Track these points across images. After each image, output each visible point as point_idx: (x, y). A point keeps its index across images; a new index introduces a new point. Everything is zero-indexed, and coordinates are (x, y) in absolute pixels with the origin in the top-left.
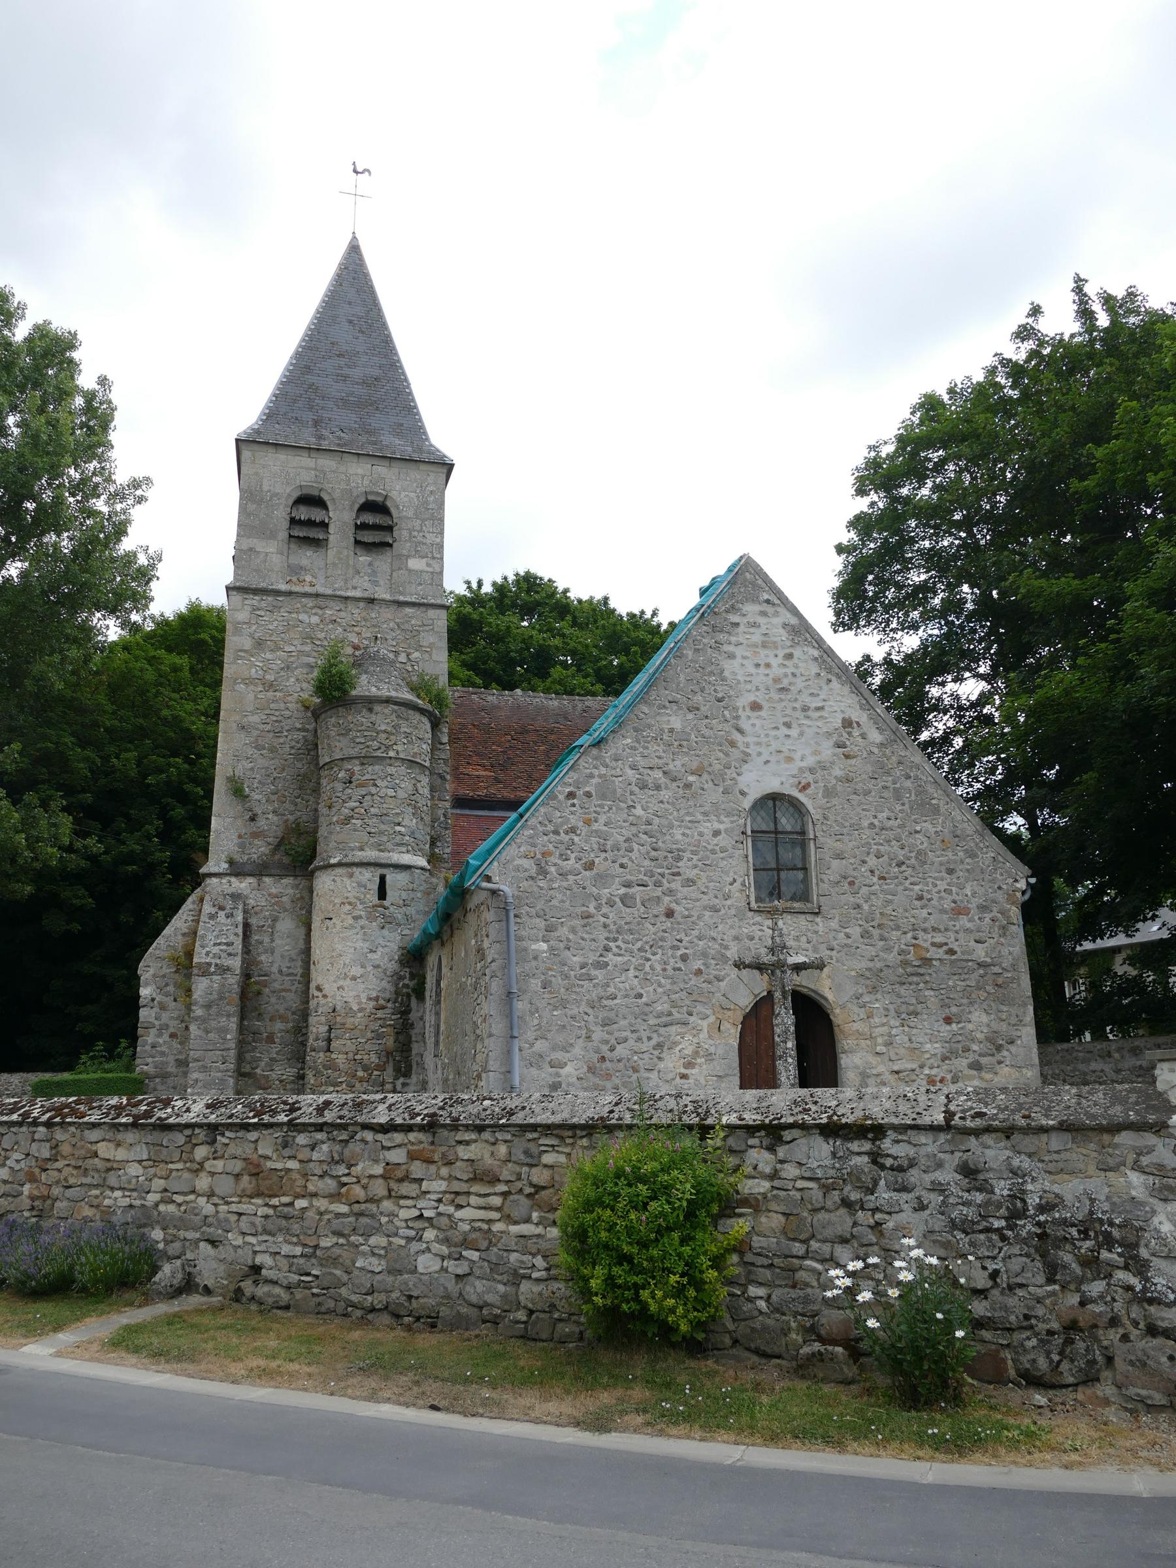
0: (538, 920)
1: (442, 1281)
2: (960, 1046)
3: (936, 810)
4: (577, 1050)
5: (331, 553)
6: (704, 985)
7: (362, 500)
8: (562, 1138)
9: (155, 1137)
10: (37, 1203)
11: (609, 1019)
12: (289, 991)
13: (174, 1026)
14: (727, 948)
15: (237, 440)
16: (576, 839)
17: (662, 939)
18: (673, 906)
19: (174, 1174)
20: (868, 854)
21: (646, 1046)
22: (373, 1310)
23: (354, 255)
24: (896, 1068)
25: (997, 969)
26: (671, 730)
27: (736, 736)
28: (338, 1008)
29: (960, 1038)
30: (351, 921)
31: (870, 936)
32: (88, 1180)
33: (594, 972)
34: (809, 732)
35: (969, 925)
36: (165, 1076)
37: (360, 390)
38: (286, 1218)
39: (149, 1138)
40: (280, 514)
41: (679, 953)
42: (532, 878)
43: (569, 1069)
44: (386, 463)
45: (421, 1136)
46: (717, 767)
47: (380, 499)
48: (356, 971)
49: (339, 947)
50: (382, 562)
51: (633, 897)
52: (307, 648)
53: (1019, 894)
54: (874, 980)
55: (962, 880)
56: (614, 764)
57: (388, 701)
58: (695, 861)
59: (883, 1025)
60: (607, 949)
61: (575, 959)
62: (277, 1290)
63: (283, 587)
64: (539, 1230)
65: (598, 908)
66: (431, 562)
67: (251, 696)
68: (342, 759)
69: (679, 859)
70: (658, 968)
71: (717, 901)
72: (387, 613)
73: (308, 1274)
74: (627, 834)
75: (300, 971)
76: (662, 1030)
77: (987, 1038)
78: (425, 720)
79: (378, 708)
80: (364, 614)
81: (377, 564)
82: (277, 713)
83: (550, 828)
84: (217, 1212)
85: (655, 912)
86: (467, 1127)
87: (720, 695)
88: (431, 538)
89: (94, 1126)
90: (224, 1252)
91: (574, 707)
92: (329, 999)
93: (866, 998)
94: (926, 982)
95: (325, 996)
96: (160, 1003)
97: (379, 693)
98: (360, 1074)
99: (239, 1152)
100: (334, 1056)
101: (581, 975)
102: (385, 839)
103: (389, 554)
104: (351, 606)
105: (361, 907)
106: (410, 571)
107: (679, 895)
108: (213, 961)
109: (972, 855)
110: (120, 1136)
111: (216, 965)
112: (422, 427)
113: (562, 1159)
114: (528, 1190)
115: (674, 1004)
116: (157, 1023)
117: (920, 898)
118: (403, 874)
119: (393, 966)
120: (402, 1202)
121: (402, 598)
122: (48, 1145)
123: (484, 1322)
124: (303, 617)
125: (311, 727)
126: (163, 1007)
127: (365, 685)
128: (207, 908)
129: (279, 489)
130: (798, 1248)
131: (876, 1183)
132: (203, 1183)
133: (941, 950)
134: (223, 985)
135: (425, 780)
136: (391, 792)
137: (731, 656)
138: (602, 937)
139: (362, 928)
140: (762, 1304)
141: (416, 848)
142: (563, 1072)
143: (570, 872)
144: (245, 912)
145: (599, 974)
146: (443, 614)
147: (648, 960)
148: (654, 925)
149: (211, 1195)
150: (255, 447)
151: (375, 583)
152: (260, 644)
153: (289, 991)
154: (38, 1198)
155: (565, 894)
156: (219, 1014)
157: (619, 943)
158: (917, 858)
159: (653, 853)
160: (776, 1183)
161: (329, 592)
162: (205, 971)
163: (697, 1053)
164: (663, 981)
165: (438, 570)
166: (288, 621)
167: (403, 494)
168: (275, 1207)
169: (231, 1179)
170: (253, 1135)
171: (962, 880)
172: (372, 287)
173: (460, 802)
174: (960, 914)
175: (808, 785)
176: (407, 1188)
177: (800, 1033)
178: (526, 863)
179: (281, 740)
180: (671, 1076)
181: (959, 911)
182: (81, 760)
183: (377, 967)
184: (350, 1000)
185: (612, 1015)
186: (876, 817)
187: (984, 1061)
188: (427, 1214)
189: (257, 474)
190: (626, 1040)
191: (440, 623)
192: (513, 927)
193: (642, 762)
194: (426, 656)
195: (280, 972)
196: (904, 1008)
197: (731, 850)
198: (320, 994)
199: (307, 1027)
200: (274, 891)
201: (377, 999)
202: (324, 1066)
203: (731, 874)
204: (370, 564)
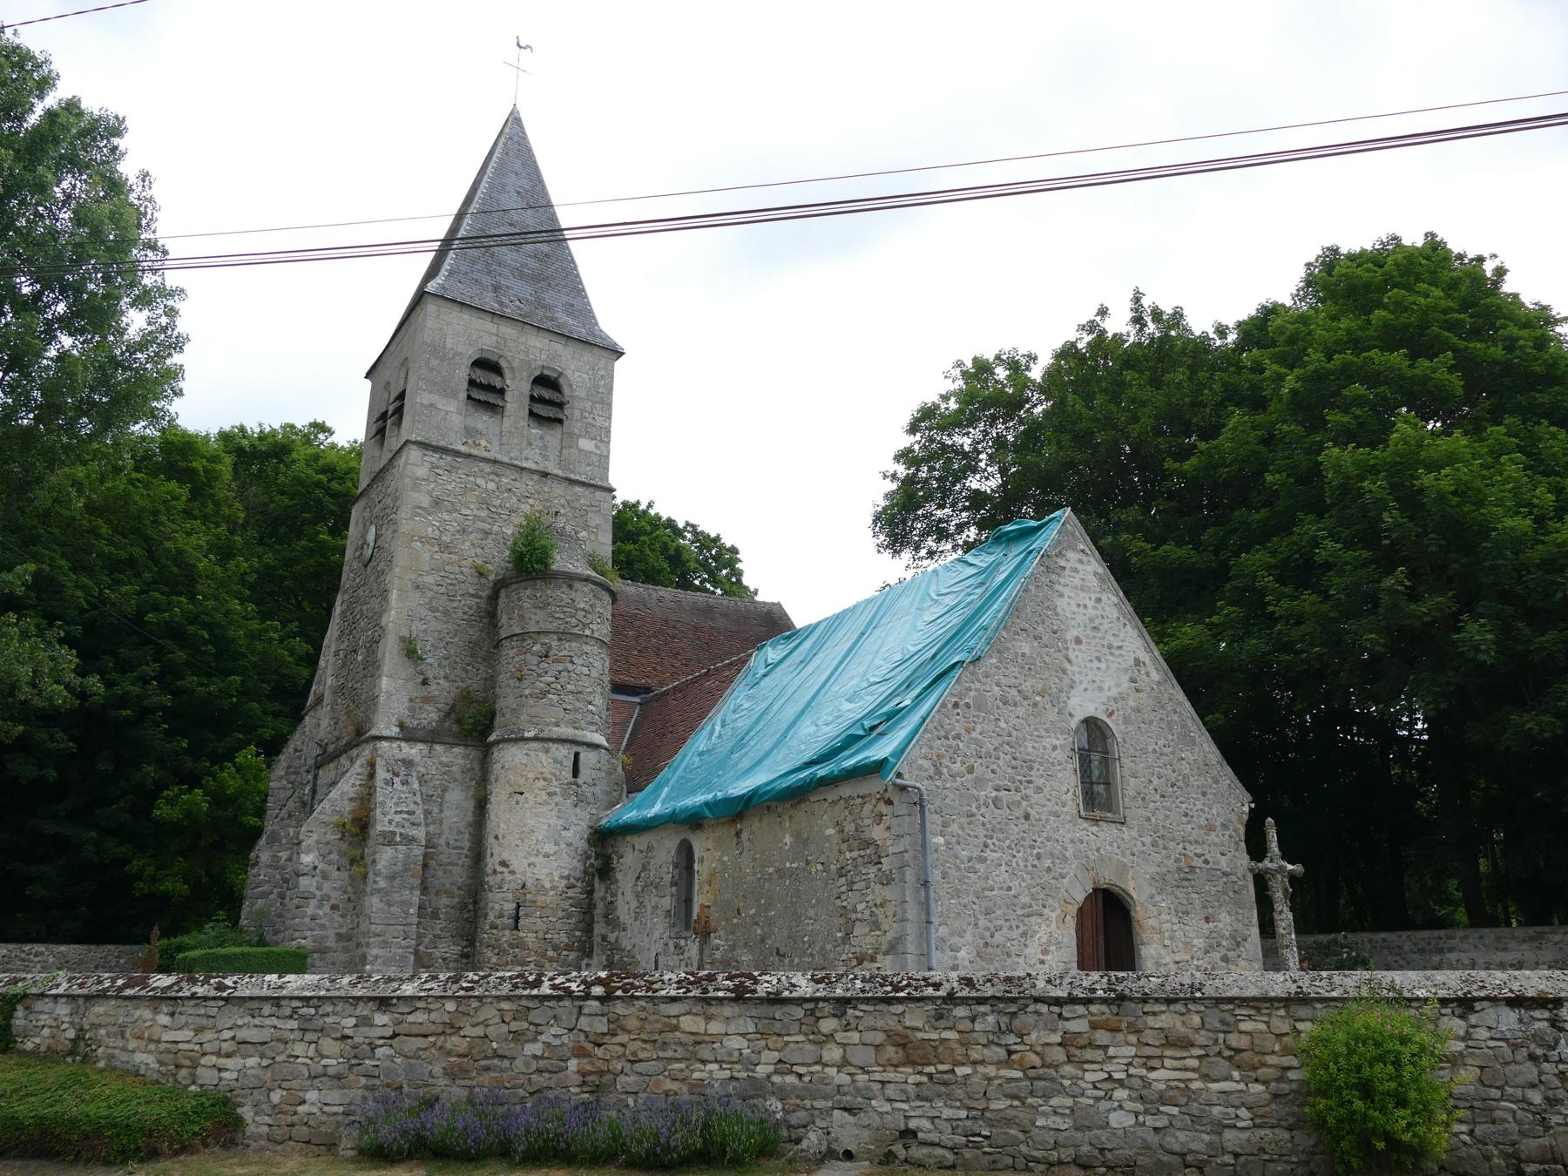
1: (1140, 1133)
3: (1193, 741)
4: (968, 936)
5: (507, 422)
8: (1258, 1009)
9: (765, 1010)
10: (590, 1078)
13: (336, 897)
19: (792, 1046)
21: (1016, 933)
22: (1060, 1163)
23: (514, 120)
25: (1234, 878)
26: (1023, 655)
27: (1066, 665)
30: (545, 797)
32: (669, 1054)
33: (978, 866)
34: (1114, 666)
37: (532, 263)
38: (945, 1084)
39: (754, 1012)
43: (962, 954)
44: (563, 341)
45: (1104, 1008)
47: (555, 375)
48: (549, 848)
49: (531, 823)
50: (553, 437)
52: (484, 514)
54: (1160, 881)
57: (587, 580)
62: (940, 1151)
63: (463, 449)
64: (1242, 1086)
65: (978, 808)
67: (427, 556)
69: (1031, 768)
70: (1022, 864)
72: (559, 489)
73: (979, 1135)
79: (578, 585)
81: (547, 438)
83: (942, 733)
84: (854, 1081)
86: (1157, 1000)
88: (600, 421)
89: (673, 999)
90: (864, 1118)
95: (512, 872)
96: (322, 872)
98: (550, 953)
99: (880, 1023)
100: (522, 934)
103: (559, 430)
104: (525, 476)
109: (1217, 782)
110: (712, 1010)
112: (591, 311)
113: (1263, 1027)
114: (1227, 1053)
116: (318, 893)
117: (1186, 815)
119: (582, 845)
120: (1086, 1066)
122: (605, 1020)
123: (1187, 1167)
124: (480, 481)
126: (325, 877)
127: (561, 562)
128: (381, 774)
130: (1495, 1093)
131: (1557, 1042)
132: (833, 1053)
137: (1061, 595)
140: (1466, 1138)
143: (958, 775)
149: (844, 1064)
150: (442, 302)
151: (545, 457)
152: (437, 502)
154: (591, 1073)
156: (403, 887)
160: (1470, 1043)
162: (389, 839)
168: (930, 1076)
169: (872, 1050)
170: (899, 1008)
172: (535, 162)
176: (1089, 1054)
177: (1108, 926)
178: (926, 764)
181: (1210, 828)
182: (76, 589)
187: (1231, 954)
188: (1116, 1076)
193: (1004, 681)
194: (593, 537)
200: (444, 759)
201: (568, 878)
202: (511, 945)
204: (542, 438)
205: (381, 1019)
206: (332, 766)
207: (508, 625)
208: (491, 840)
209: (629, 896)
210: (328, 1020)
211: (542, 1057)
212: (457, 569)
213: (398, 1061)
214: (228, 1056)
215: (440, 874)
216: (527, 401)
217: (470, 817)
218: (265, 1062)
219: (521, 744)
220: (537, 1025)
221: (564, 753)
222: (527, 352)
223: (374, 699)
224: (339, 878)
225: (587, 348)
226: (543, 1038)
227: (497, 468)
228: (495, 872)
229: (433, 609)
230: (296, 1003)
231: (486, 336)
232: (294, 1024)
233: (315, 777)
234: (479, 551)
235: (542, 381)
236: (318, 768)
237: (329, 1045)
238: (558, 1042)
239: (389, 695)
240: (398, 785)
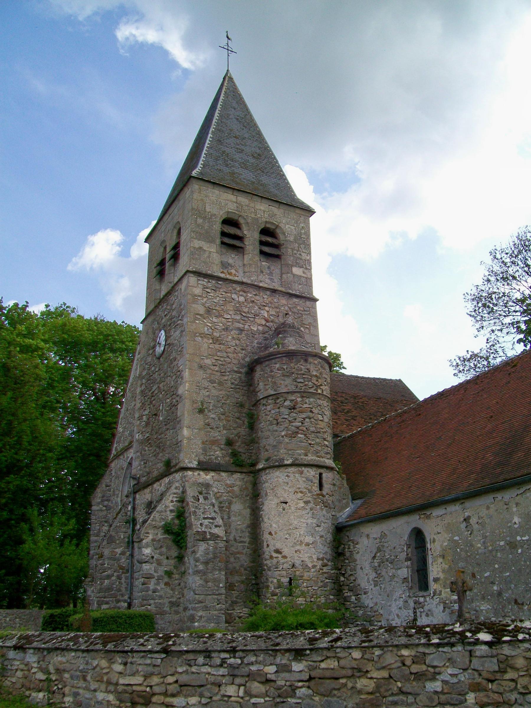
6: (301, 556)
12: (242, 553)
28: (297, 565)
30: (302, 505)
44: (277, 205)
47: (273, 227)
48: (309, 539)
50: (276, 267)
52: (238, 317)
63: (222, 275)
66: (305, 271)
67: (206, 345)
68: (288, 393)
79: (310, 360)
80: (270, 299)
82: (222, 359)
92: (289, 559)
95: (285, 557)
96: (157, 560)
102: (319, 448)
105: (309, 495)
106: (294, 275)
108: (206, 530)
111: (210, 533)
116: (155, 574)
122: (495, 660)
124: (234, 296)
129: (215, 211)
134: (216, 548)
139: (311, 509)
150: (202, 183)
152: (209, 311)
153: (242, 553)
156: (214, 569)
166: (225, 298)
167: (287, 226)
179: (226, 378)
183: (322, 537)
184: (307, 559)
189: (202, 200)
195: (235, 540)
198: (280, 556)
200: (228, 482)
201: (322, 559)
204: (269, 268)
205: (297, 667)
206: (147, 490)
207: (263, 389)
208: (266, 536)
209: (367, 569)
210: (254, 668)
211: (442, 693)
213: (317, 698)
214: (173, 695)
216: (257, 244)
217: (248, 522)
218: (204, 701)
219: (282, 469)
220: (434, 667)
221: (312, 473)
222: (257, 213)
223: (178, 444)
224: (168, 564)
225: (292, 209)
226: (441, 677)
228: (271, 557)
230: (224, 655)
232: (222, 671)
233: (134, 499)
234: (237, 342)
235: (265, 232)
236: (135, 493)
237: (256, 687)
238: (455, 680)
239: (189, 439)
240: (201, 500)
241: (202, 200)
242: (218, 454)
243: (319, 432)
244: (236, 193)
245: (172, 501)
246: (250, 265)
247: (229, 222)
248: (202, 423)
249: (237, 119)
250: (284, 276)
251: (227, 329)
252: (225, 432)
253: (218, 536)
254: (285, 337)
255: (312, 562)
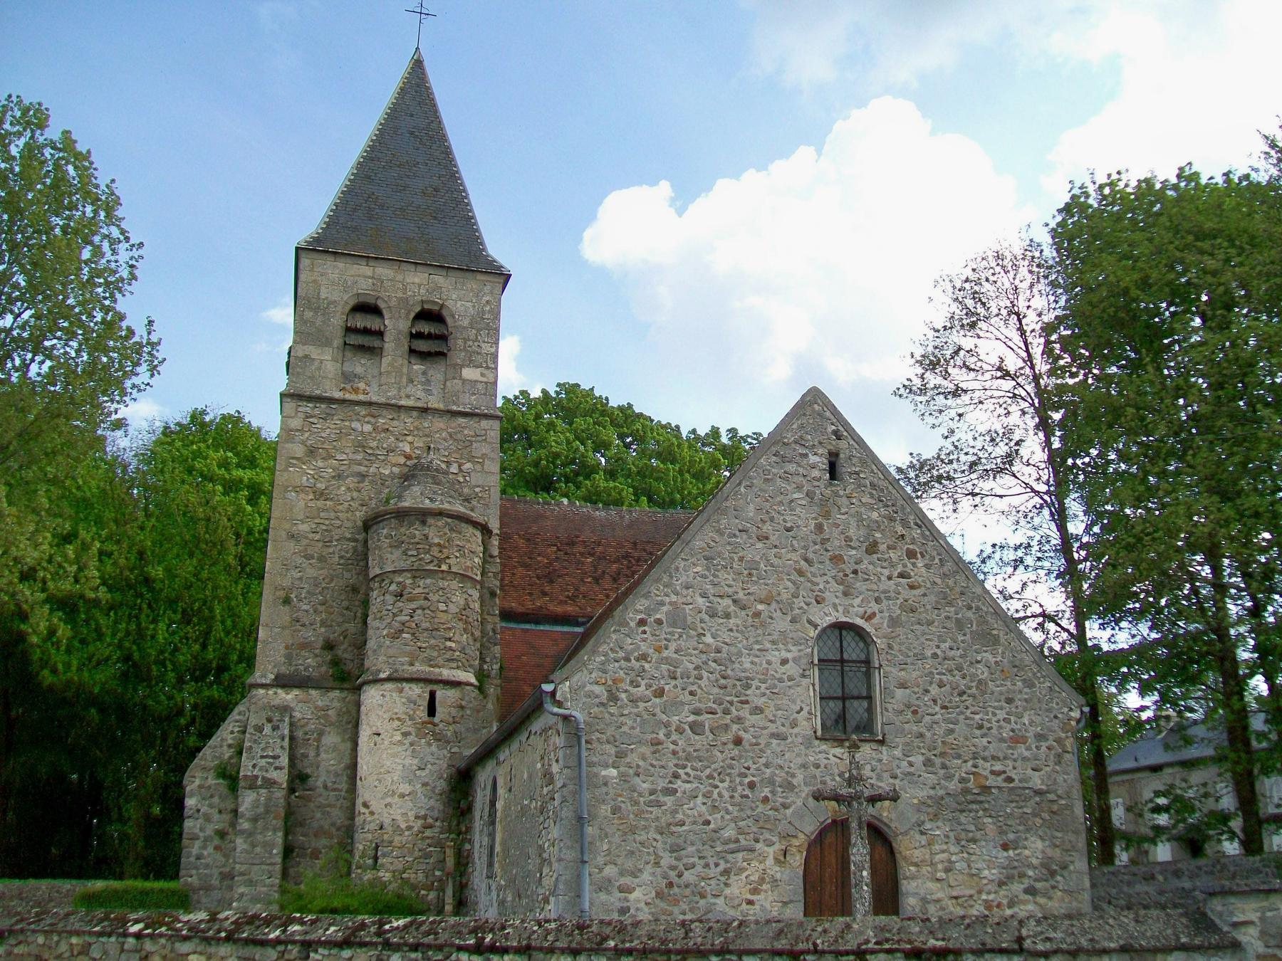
0: (608, 746)
2: (1015, 872)
3: (996, 640)
4: (646, 876)
6: (770, 812)
7: (418, 309)
11: (678, 845)
12: (334, 806)
14: (793, 776)
15: (297, 249)
16: (647, 666)
17: (731, 767)
18: (741, 733)
20: (931, 683)
24: (955, 894)
25: (1052, 797)
28: (385, 825)
29: (1016, 864)
30: (398, 737)
31: (933, 765)
35: (1027, 754)
36: (208, 888)
40: (337, 320)
41: (747, 780)
42: (603, 704)
46: (785, 596)
47: (436, 308)
48: (405, 788)
50: (437, 372)
51: (702, 725)
52: (359, 457)
53: (1073, 723)
54: (935, 808)
55: (1020, 709)
56: (685, 592)
57: (441, 514)
58: (763, 690)
59: (943, 852)
60: (676, 776)
61: (645, 785)
63: (338, 395)
65: (668, 735)
66: (485, 372)
67: (302, 504)
68: (394, 572)
69: (748, 687)
70: (726, 794)
71: (784, 729)
72: (439, 423)
74: (698, 661)
75: (344, 786)
76: (730, 857)
77: (1043, 865)
78: (478, 534)
79: (430, 521)
81: (431, 372)
83: (621, 654)
85: (724, 739)
87: (788, 525)
88: (486, 348)
91: (622, 517)
92: (376, 816)
93: (928, 826)
94: (985, 810)
95: (372, 813)
97: (433, 506)
101: (651, 801)
102: (435, 654)
103: (443, 363)
106: (464, 381)
107: (747, 723)
109: (1031, 686)
111: (263, 778)
115: (741, 831)
116: (201, 834)
117: (980, 727)
118: (453, 691)
119: (441, 785)
121: (455, 408)
124: (356, 425)
125: (361, 537)
129: (335, 296)
133: (1000, 779)
135: (476, 594)
136: (442, 607)
138: (671, 764)
139: (411, 744)
141: (466, 664)
142: (632, 896)
144: (291, 724)
145: (669, 801)
146: (496, 425)
147: (716, 787)
148: (722, 752)
150: (315, 255)
151: (428, 392)
152: (312, 452)
155: (635, 721)
156: (266, 829)
157: (688, 770)
158: (977, 688)
159: (723, 681)
161: (383, 400)
163: (763, 879)
164: (730, 808)
165: (492, 380)
166: (340, 429)
167: (459, 303)
171: (1020, 709)
173: (507, 615)
174: (1018, 742)
175: (874, 614)
178: (598, 689)
179: (331, 550)
180: (736, 902)
181: (1017, 739)
184: (399, 817)
185: (680, 841)
186: (938, 647)
187: (1039, 885)
190: (693, 866)
191: (492, 434)
192: (584, 754)
193: (711, 590)
194: (478, 467)
195: (325, 787)
196: (963, 835)
197: (798, 679)
198: (366, 811)
199: (352, 843)
200: (320, 703)
201: (425, 817)
203: (799, 702)
204: (424, 373)
212: (332, 515)
215: (318, 815)
219: (378, 686)
221: (416, 691)
227: (374, 410)
229: (308, 557)
231: (361, 280)
234: (355, 494)
241: (315, 281)
242: (310, 663)
243: (437, 629)
244: (372, 263)
245: (232, 732)
246: (388, 373)
247: (367, 308)
248: (288, 618)
249: (412, 133)
250: (448, 383)
251: (339, 476)
252: (323, 630)
253: (275, 783)
254: (410, 485)
255: (407, 821)
